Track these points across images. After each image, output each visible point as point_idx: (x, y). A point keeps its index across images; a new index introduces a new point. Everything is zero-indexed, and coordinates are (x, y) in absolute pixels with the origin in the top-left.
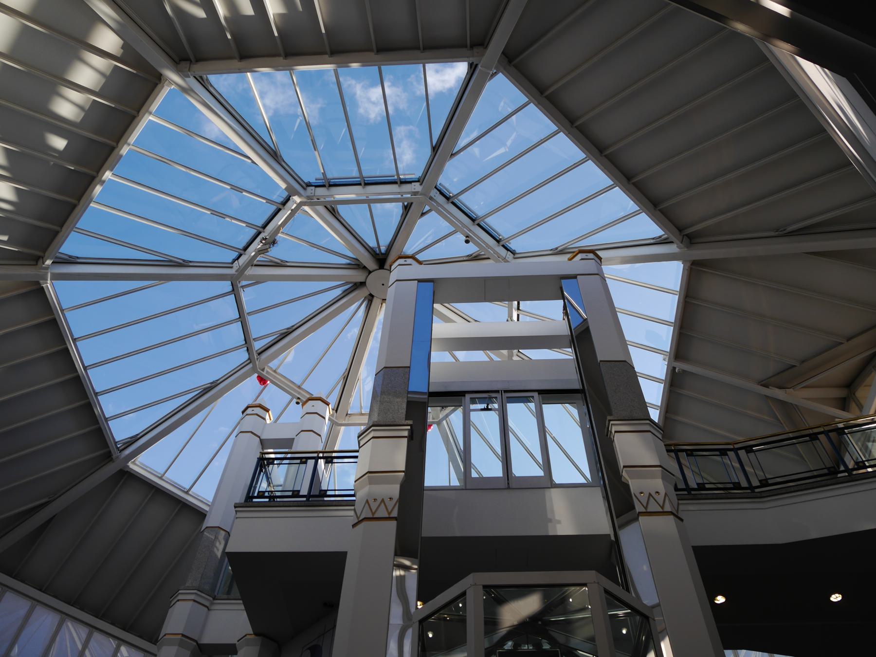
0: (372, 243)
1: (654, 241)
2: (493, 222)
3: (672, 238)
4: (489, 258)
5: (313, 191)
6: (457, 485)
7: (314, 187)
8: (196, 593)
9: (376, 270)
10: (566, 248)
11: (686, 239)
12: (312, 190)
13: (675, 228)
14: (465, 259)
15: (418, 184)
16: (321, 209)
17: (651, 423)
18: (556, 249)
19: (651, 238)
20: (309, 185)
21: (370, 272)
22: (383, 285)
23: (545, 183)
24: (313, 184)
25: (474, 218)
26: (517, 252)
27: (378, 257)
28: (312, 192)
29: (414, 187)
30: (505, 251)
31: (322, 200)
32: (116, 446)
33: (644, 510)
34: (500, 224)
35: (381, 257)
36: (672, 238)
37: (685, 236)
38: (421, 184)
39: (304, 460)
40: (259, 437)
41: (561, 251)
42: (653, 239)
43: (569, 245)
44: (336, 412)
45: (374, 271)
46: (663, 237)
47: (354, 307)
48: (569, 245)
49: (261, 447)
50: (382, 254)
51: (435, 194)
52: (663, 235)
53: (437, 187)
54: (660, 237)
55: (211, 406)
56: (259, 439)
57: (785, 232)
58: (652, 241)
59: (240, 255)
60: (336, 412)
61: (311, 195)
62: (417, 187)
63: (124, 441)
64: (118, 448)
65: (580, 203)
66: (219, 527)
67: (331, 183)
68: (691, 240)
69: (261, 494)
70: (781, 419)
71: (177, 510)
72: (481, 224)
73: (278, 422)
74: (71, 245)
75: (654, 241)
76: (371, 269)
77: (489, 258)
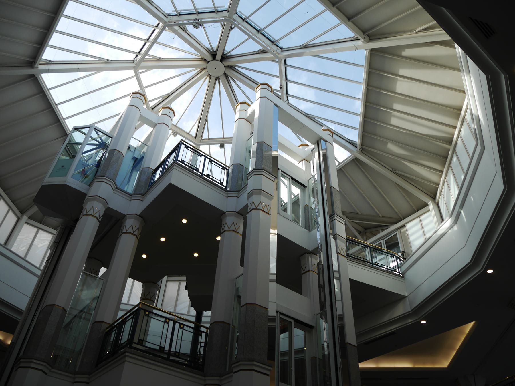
0: (208, 46)
1: (258, 52)
2: (269, 31)
3: (359, 37)
4: (268, 52)
5: (171, 18)
7: (171, 16)
8: (237, 193)
11: (367, 38)
12: (170, 18)
13: (360, 31)
15: (226, 12)
16: (177, 28)
18: (303, 45)
19: (256, 50)
20: (169, 15)
21: (208, 62)
22: (216, 69)
24: (171, 15)
25: (259, 30)
26: (283, 48)
27: (212, 53)
28: (170, 19)
29: (224, 14)
30: (276, 47)
31: (177, 23)
32: (84, 158)
33: (150, 298)
34: (274, 32)
35: (213, 53)
36: (359, 37)
37: (366, 36)
38: (228, 12)
40: (244, 119)
41: (305, 46)
42: (351, 38)
44: (196, 138)
45: (210, 61)
46: (304, 45)
47: (201, 81)
50: (214, 52)
51: (236, 17)
52: (355, 36)
53: (237, 13)
54: (354, 37)
59: (137, 56)
60: (196, 138)
61: (170, 20)
62: (226, 14)
63: (88, 156)
64: (85, 160)
66: (239, 164)
67: (199, 12)
68: (369, 37)
70: (431, 141)
71: (386, 75)
72: (262, 33)
73: (124, 156)
74: (48, 54)
75: (258, 52)
76: (209, 61)
77: (268, 52)
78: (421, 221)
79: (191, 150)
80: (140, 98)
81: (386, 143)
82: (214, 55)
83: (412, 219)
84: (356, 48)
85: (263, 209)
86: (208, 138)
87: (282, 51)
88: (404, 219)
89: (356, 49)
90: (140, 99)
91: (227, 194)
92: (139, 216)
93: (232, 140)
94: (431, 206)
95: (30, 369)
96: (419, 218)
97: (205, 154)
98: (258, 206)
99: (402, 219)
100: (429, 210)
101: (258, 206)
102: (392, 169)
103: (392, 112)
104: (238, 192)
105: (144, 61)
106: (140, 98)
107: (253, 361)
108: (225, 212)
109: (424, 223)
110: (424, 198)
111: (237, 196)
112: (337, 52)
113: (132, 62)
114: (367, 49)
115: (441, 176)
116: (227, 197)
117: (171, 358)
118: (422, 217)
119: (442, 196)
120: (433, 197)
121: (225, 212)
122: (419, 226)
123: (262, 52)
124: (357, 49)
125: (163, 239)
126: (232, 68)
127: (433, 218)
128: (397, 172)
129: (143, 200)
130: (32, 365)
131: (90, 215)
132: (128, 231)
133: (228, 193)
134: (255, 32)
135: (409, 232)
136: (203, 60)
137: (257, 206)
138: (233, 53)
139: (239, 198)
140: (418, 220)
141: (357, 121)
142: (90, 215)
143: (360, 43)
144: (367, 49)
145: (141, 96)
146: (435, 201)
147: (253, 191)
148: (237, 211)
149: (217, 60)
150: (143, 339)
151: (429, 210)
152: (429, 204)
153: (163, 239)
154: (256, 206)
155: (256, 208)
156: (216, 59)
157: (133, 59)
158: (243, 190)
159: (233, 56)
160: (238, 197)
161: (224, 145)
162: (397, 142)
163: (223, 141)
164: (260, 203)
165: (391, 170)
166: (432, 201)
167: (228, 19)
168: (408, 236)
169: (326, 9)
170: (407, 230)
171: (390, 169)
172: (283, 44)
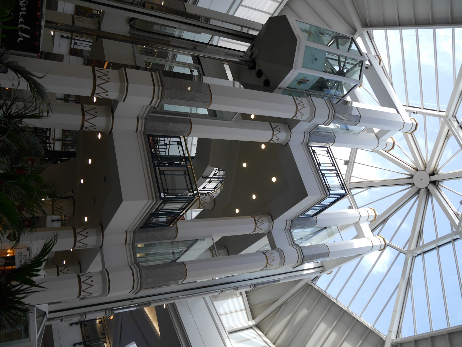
6: (189, 74)
9: (428, 186)
10: (410, 285)
14: (421, 229)
17: (138, 291)
18: (411, 280)
22: (421, 179)
23: (456, 261)
34: (431, 256)
35: (437, 183)
39: (328, 152)
40: (359, 220)
42: (411, 276)
43: (411, 288)
45: (429, 184)
48: (411, 288)
49: (354, 223)
55: (379, 103)
56: (358, 221)
57: (285, 303)
58: (410, 276)
65: (441, 274)
69: (323, 174)
71: (361, 342)
78: (242, 310)
79: (341, 183)
80: (410, 130)
81: (308, 310)
82: (434, 183)
83: (245, 303)
84: (391, 332)
85: (296, 117)
86: (355, 162)
87: (413, 256)
88: (246, 295)
89: (390, 331)
90: (409, 131)
91: (290, 221)
92: (288, 143)
93: (354, 149)
94: (252, 323)
95: (153, 87)
96: (245, 309)
97: (339, 169)
98: (300, 112)
99: (247, 294)
100: (249, 321)
101: (300, 112)
102: (287, 303)
103: (331, 328)
104: (289, 230)
105: (449, 129)
106: (410, 130)
107: (139, 268)
108: (273, 221)
109: (240, 313)
110: (258, 319)
111: (304, 142)
112: (393, 311)
113: (454, 115)
114: (386, 339)
115: (271, 340)
116: (287, 221)
117: (157, 168)
118: (244, 312)
119: (256, 336)
120: (258, 326)
121: (273, 221)
122: (238, 309)
123: (420, 235)
124: (390, 331)
125: (254, 197)
126: (418, 191)
127: (242, 324)
128: (284, 306)
129: (302, 144)
130: (157, 88)
131: (297, 106)
132: (275, 136)
133: (291, 222)
134: (440, 244)
135: (235, 299)
136: (434, 170)
137: (269, 257)
138: (430, 199)
139: (301, 145)
140: (243, 307)
141: (332, 293)
142: (297, 106)
143: (393, 337)
144: (386, 339)
145: (411, 132)
146: (254, 326)
147: (284, 258)
148: (289, 143)
149: (430, 178)
150: (167, 189)
151: (249, 321)
152: (253, 321)
153: (254, 197)
154: (300, 110)
155: (298, 109)
156: (431, 177)
157: (456, 116)
158: (289, 236)
159: (427, 198)
160: (302, 143)
161: (347, 165)
162: (306, 319)
163: (351, 162)
164: (303, 114)
165: (287, 302)
166: (255, 324)
167: (459, 231)
168: (232, 298)
169: (432, 330)
170: (237, 297)
171: (287, 301)
172: (419, 259)
